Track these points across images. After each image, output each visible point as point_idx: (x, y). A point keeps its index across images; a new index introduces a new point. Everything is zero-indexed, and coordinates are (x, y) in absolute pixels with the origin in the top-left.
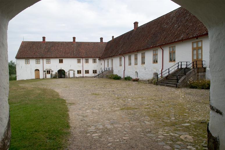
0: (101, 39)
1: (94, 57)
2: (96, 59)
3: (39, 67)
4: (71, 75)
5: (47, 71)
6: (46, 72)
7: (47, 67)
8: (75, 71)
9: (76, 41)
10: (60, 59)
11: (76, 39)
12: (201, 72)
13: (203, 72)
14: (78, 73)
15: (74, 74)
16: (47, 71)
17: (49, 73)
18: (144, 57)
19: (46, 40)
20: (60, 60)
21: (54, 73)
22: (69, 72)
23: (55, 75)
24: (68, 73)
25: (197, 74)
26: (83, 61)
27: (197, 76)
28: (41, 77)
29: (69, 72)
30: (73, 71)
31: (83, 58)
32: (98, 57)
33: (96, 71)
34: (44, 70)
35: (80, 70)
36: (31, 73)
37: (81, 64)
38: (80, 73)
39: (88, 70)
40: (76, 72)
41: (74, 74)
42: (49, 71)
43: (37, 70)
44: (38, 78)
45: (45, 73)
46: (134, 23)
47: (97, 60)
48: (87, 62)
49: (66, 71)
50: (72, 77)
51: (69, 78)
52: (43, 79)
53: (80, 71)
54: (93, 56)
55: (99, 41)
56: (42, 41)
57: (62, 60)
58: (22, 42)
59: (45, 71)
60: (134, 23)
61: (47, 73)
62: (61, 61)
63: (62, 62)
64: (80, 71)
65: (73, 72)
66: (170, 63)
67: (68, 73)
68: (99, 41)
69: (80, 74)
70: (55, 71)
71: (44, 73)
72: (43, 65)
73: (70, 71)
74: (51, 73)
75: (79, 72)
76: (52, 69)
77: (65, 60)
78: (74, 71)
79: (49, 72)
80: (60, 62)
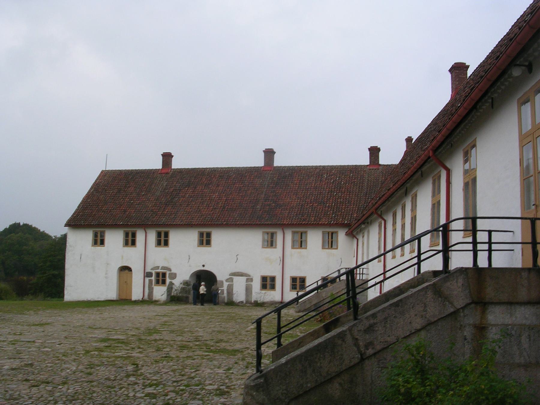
0: (374, 152)
1: (330, 225)
2: (337, 232)
3: (133, 257)
4: (239, 295)
5: (158, 274)
6: (153, 278)
7: (159, 257)
8: (252, 280)
9: (381, 162)
10: (160, 229)
11: (381, 153)
12: (510, 303)
13: (529, 303)
14: (264, 287)
15: (248, 290)
16: (158, 274)
17: (164, 282)
18: (396, 223)
19: (176, 164)
20: (201, 235)
21: (177, 283)
22: (230, 280)
23: (183, 289)
24: (226, 284)
25: (470, 319)
26: (285, 238)
27: (468, 332)
28: (137, 294)
29: (230, 280)
30: (244, 279)
31: (283, 226)
32: (342, 225)
33: (303, 280)
34: (148, 270)
35: (272, 274)
36: (106, 278)
37: (275, 253)
38: (273, 287)
39: (302, 275)
40: (256, 285)
41: (248, 290)
42: (164, 275)
43: (125, 269)
44: (124, 300)
45: (151, 281)
46: (450, 71)
47: (341, 235)
48: (300, 243)
49: (219, 278)
50: (242, 302)
51: (231, 303)
52: (143, 302)
53: (273, 279)
54: (323, 221)
55: (364, 160)
56: (160, 167)
57: (209, 235)
58: (102, 172)
59: (149, 275)
60: (450, 71)
61: (157, 282)
62: (205, 240)
63: (208, 243)
64: (273, 279)
65: (247, 280)
66: (199, 248)
67: (226, 284)
68: (364, 160)
69: (272, 292)
70: (183, 274)
71: (147, 279)
72: (145, 254)
73: (236, 279)
74: (168, 281)
75: (268, 283)
76: (172, 268)
77: (219, 237)
78: (250, 280)
79: (161, 278)
80: (126, 244)
